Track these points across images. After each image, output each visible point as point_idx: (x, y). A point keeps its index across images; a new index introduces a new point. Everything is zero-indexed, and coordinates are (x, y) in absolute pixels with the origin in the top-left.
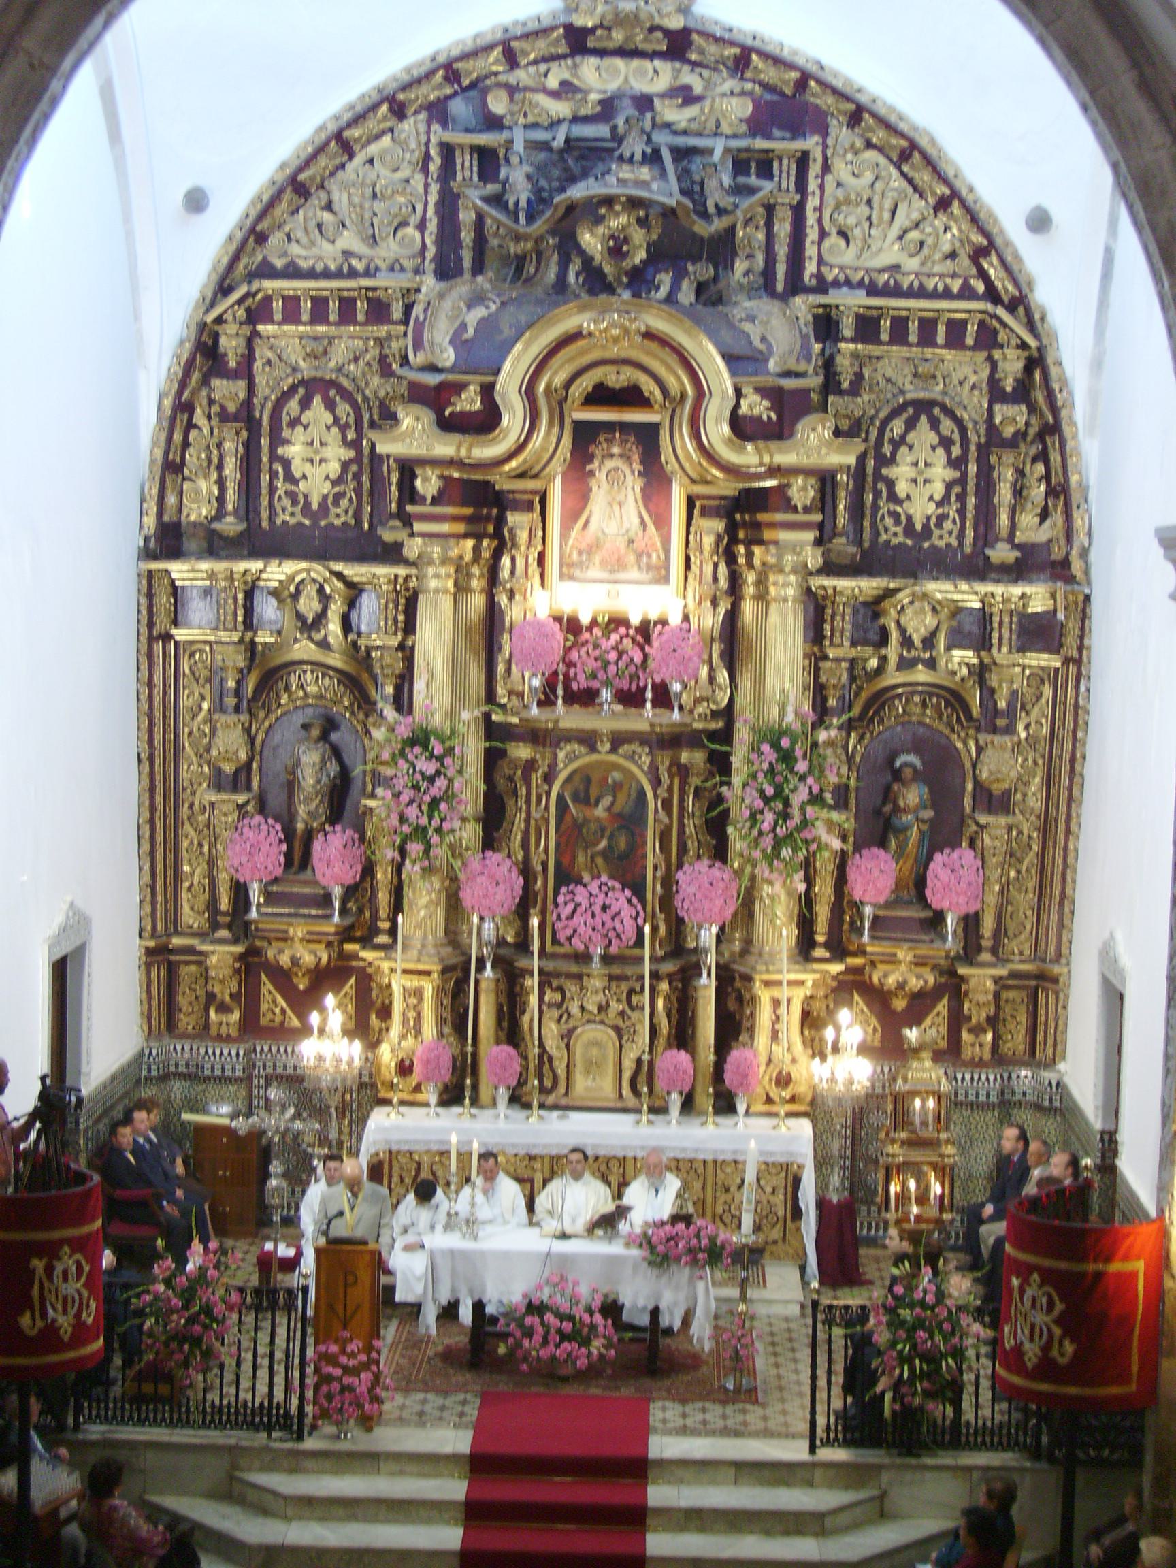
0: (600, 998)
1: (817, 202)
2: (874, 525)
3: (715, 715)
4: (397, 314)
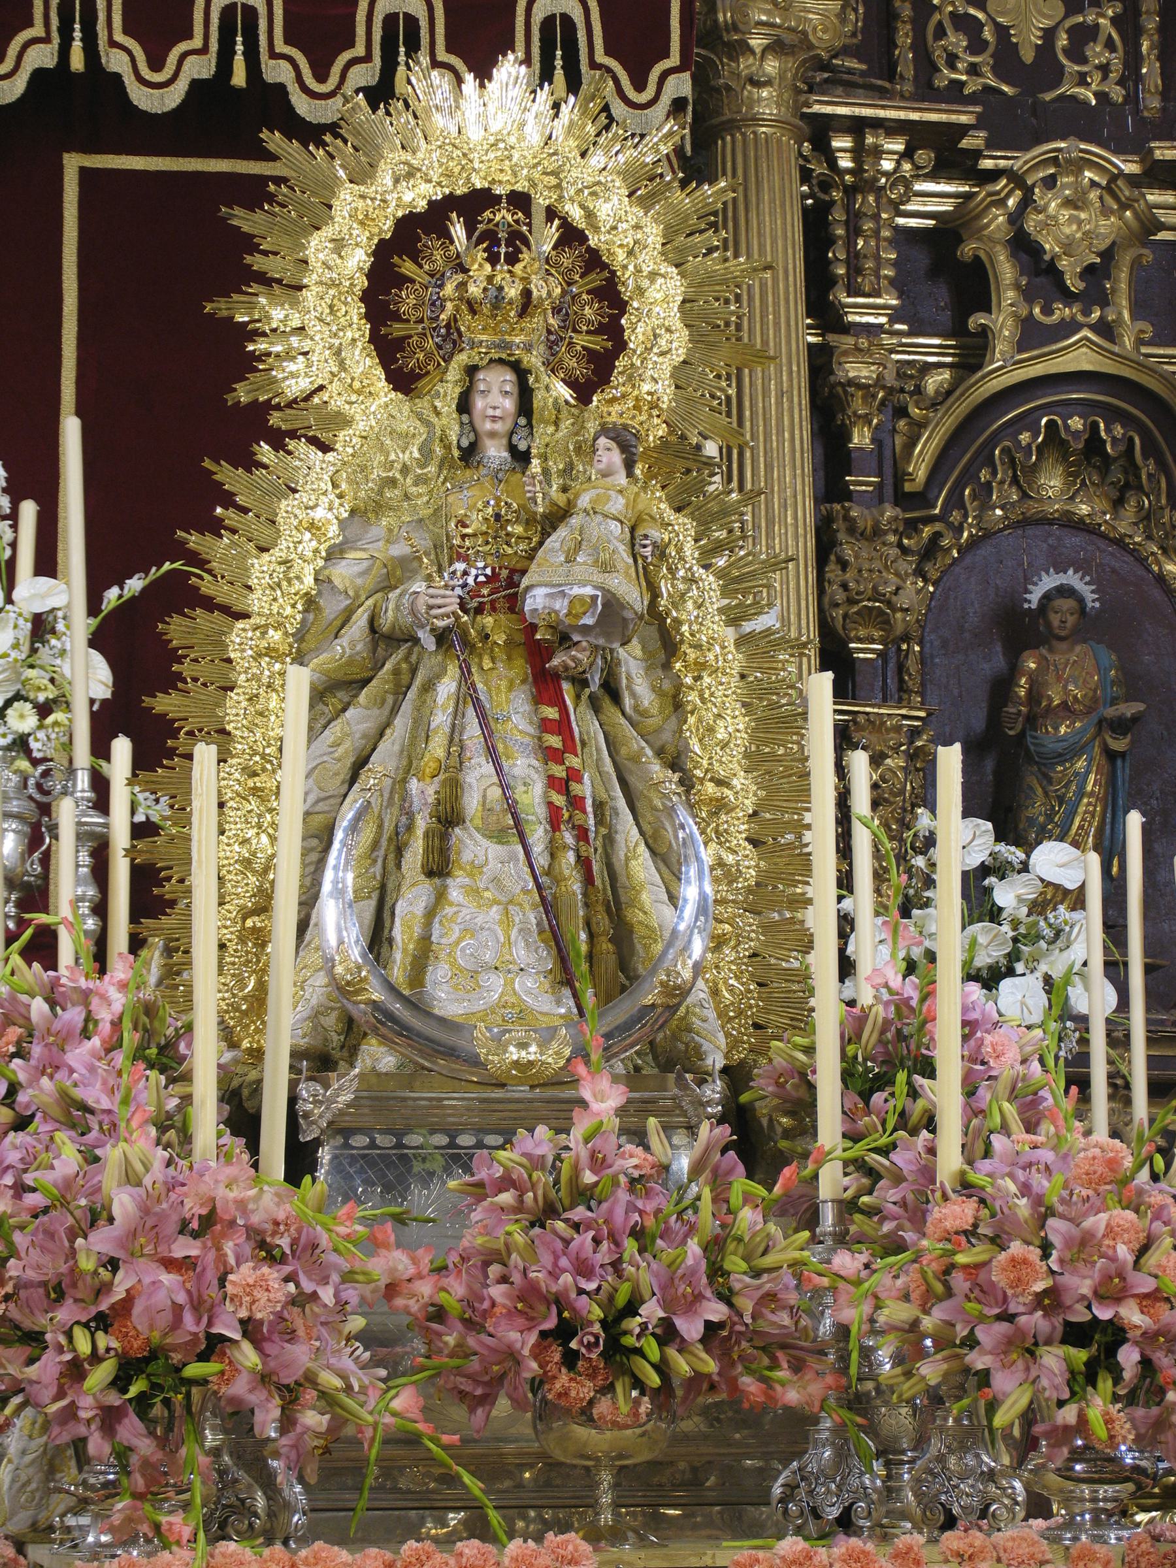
2: (921, 48)
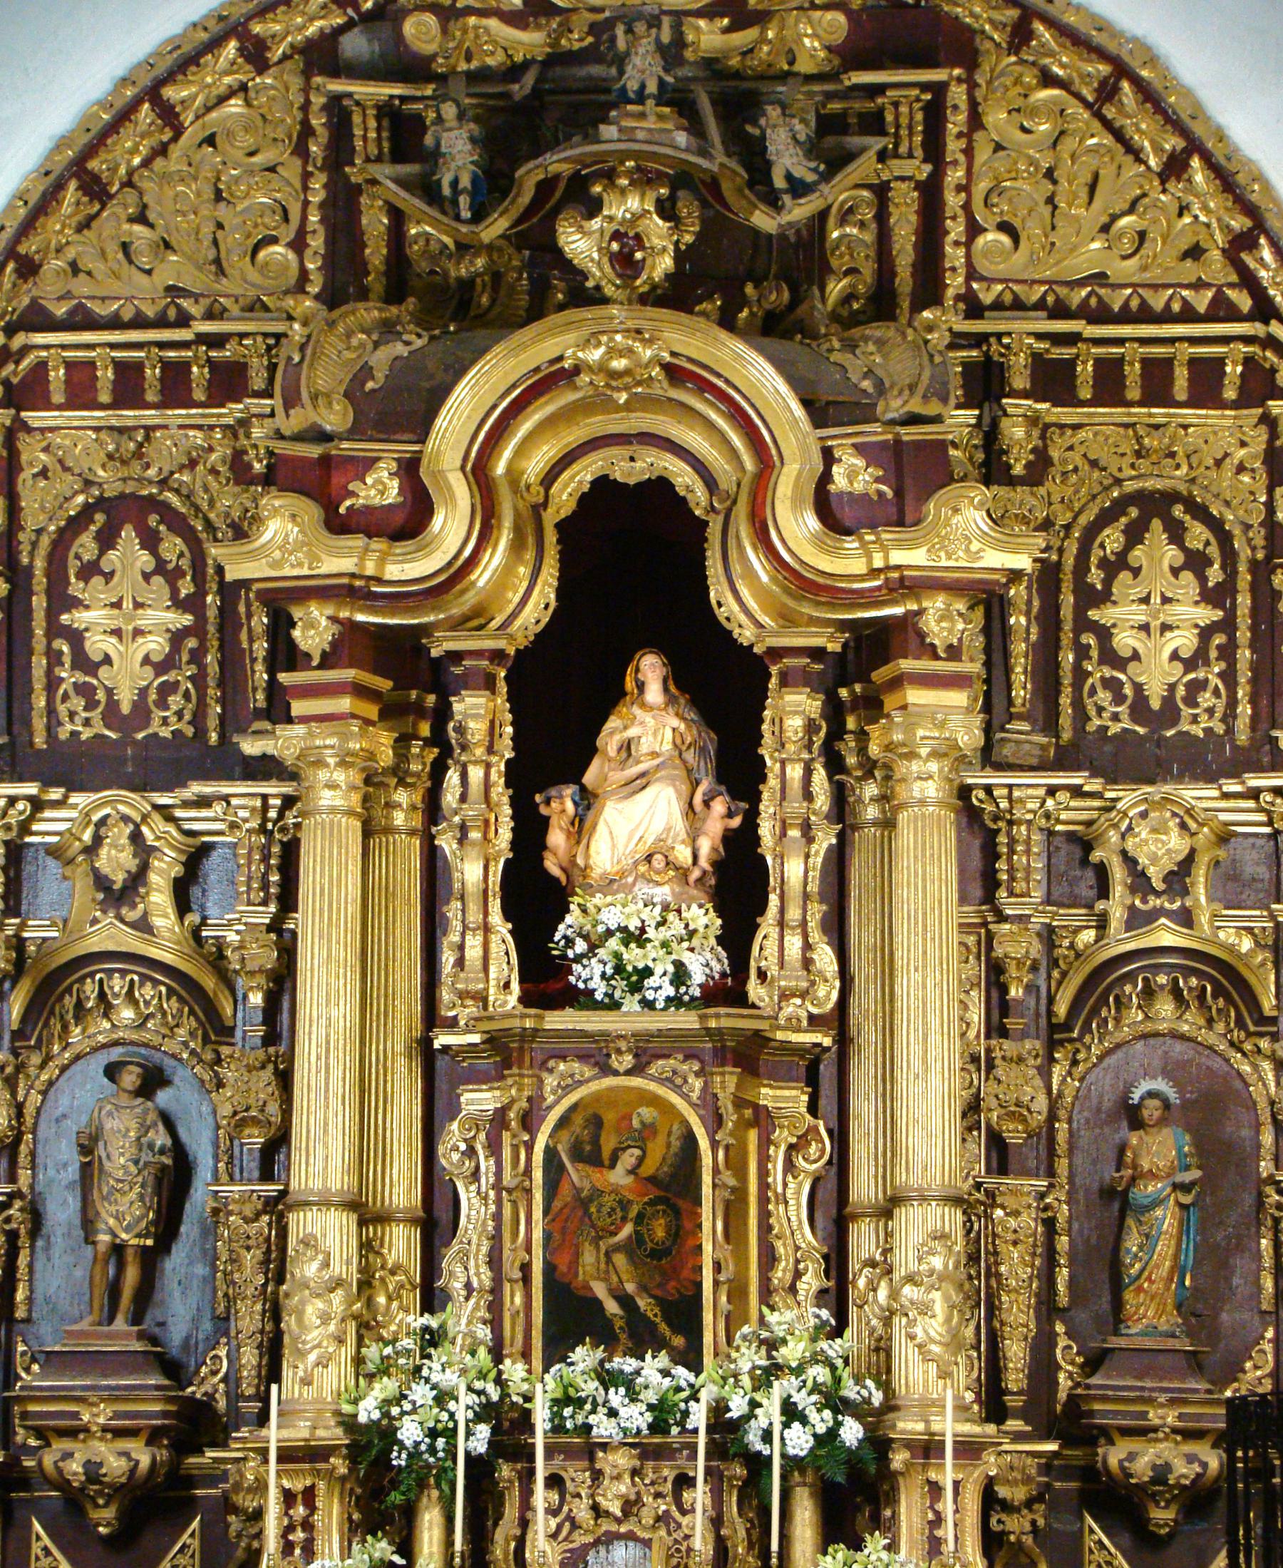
0: (623, 1488)
1: (960, 174)
2: (1078, 704)
3: (815, 1022)
4: (258, 383)
